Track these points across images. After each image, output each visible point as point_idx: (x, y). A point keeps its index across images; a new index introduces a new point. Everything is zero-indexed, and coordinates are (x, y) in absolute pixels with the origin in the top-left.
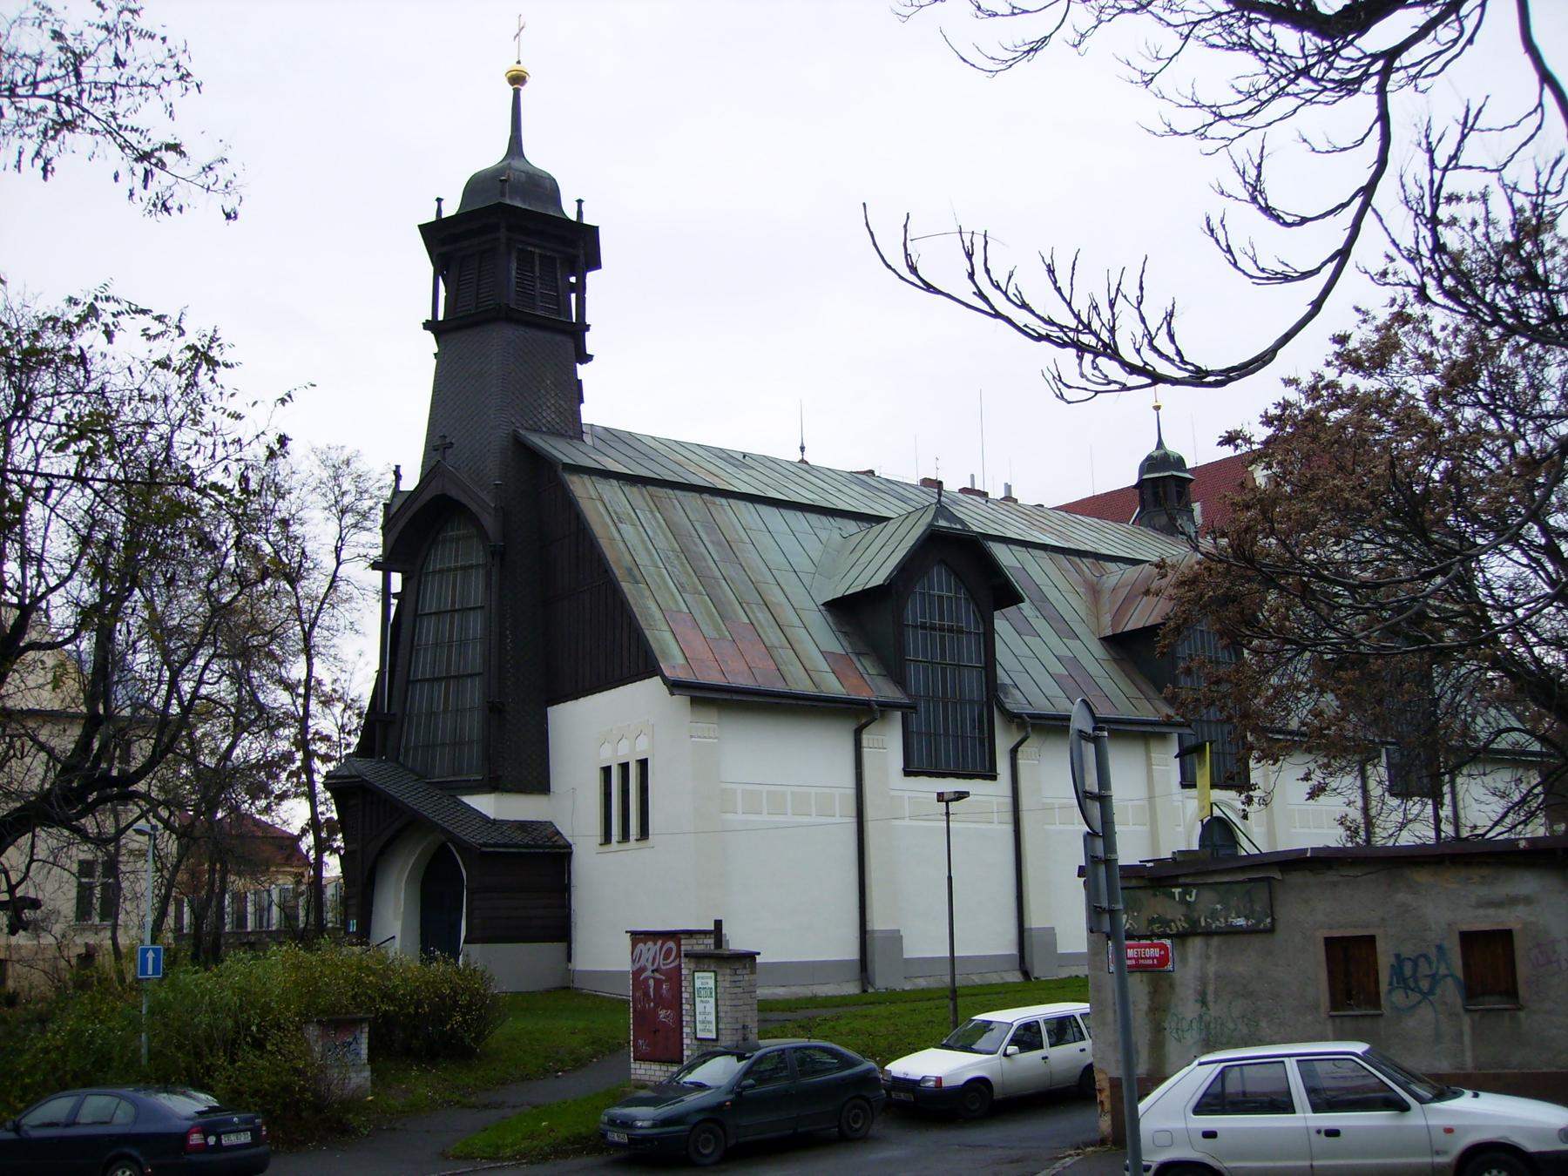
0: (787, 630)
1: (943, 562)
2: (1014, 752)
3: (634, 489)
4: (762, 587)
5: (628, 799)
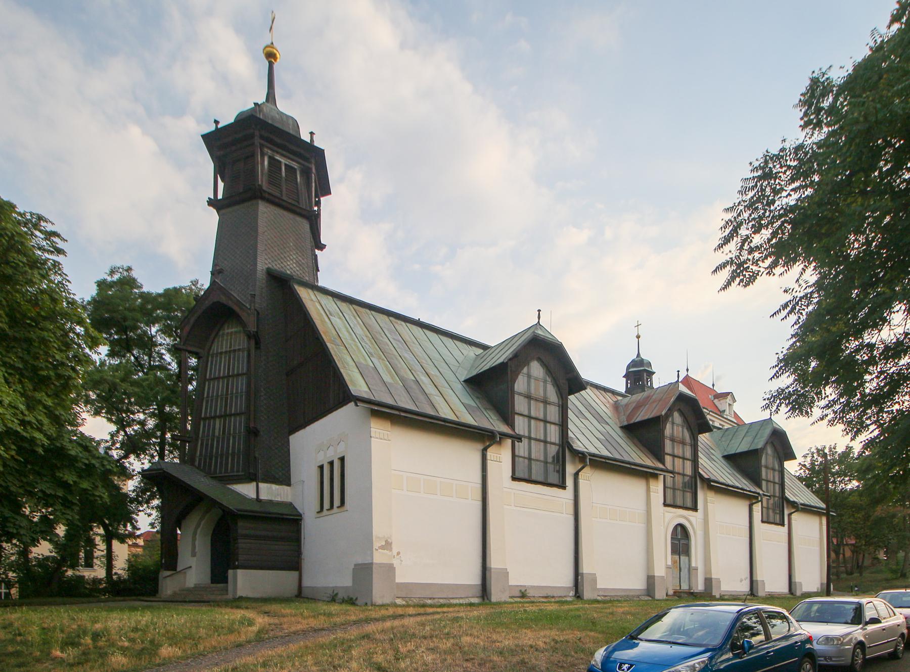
1: (539, 360)
2: (576, 475)
5: (335, 484)
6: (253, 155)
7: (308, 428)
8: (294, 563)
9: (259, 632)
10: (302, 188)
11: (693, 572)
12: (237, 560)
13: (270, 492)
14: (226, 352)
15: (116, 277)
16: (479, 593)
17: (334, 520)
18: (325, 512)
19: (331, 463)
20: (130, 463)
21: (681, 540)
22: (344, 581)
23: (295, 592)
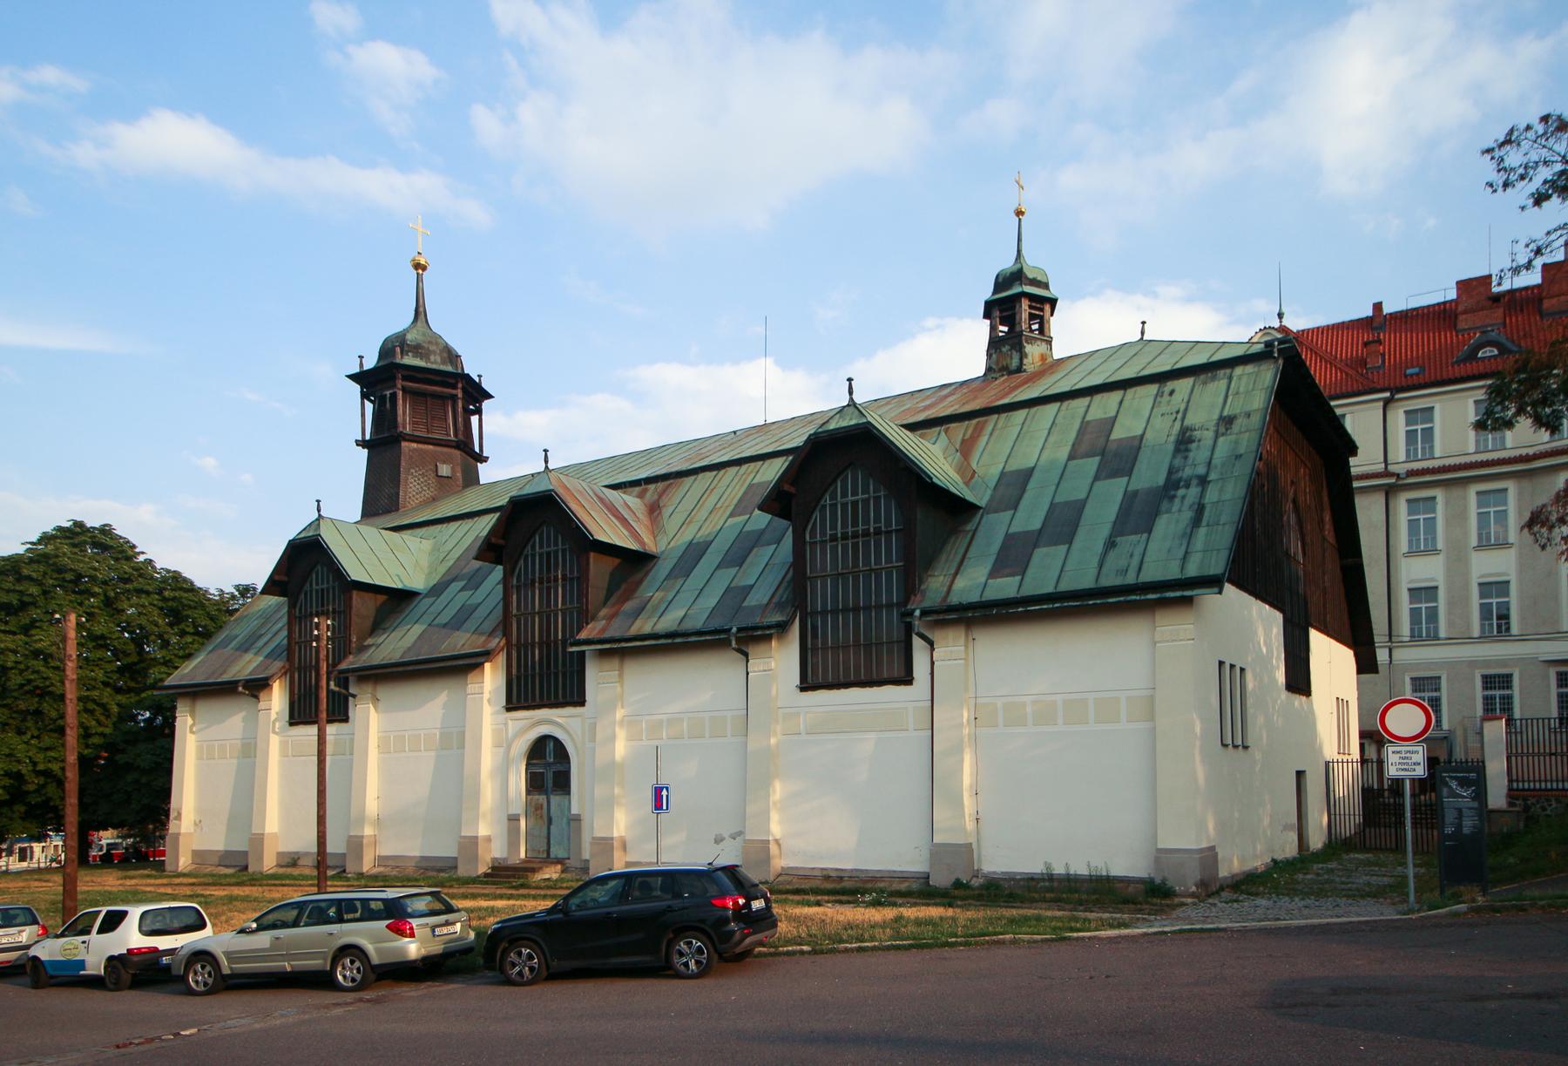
21: (549, 768)
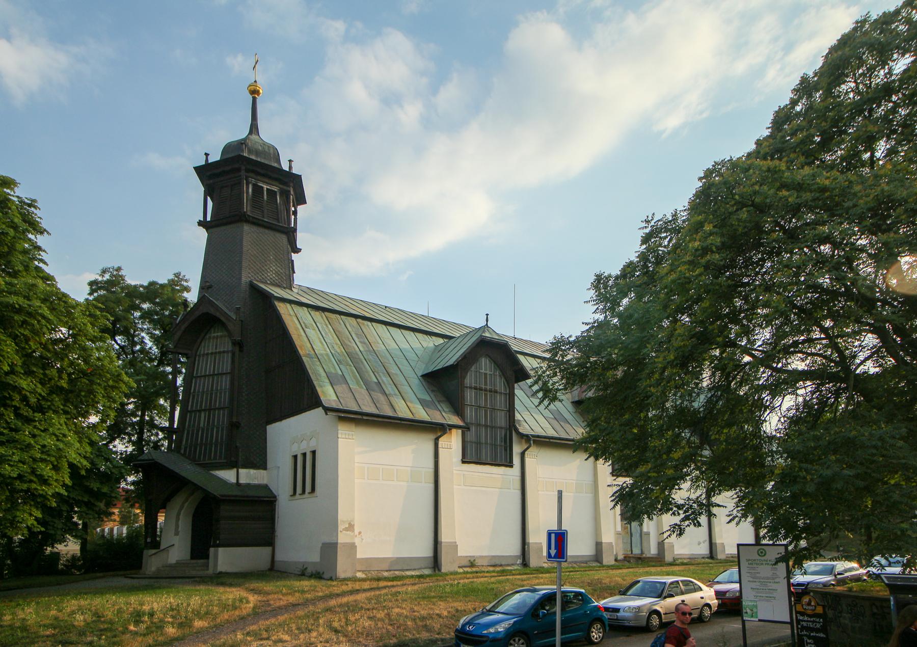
0: (399, 386)
1: (487, 356)
2: (523, 455)
3: (317, 313)
4: (386, 365)
5: (308, 472)
6: (240, 183)
7: (284, 421)
8: (268, 539)
9: (254, 608)
10: (282, 208)
11: (644, 537)
12: (219, 539)
13: (248, 476)
14: (212, 353)
15: (107, 277)
16: (431, 565)
17: (305, 503)
18: (297, 496)
19: (304, 455)
20: (114, 447)
22: (313, 557)
23: (268, 565)
